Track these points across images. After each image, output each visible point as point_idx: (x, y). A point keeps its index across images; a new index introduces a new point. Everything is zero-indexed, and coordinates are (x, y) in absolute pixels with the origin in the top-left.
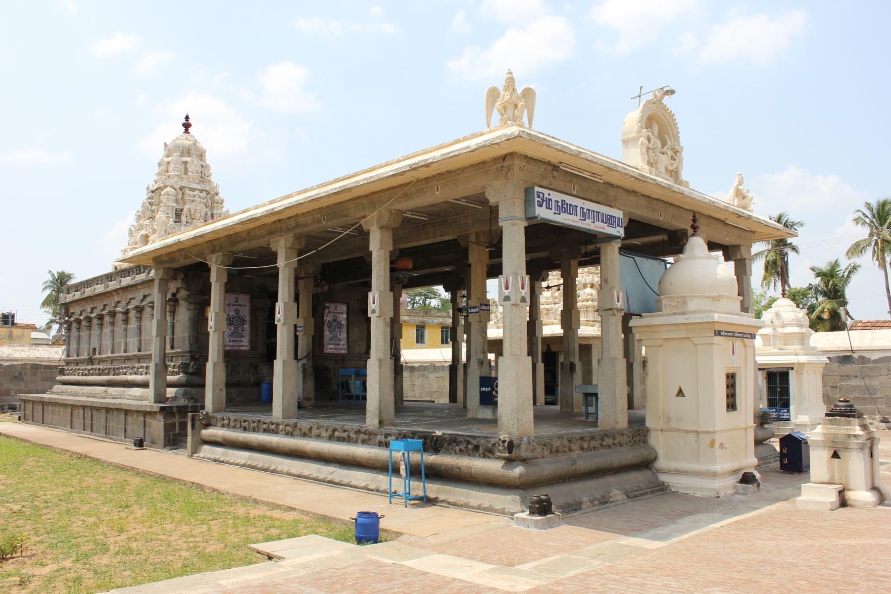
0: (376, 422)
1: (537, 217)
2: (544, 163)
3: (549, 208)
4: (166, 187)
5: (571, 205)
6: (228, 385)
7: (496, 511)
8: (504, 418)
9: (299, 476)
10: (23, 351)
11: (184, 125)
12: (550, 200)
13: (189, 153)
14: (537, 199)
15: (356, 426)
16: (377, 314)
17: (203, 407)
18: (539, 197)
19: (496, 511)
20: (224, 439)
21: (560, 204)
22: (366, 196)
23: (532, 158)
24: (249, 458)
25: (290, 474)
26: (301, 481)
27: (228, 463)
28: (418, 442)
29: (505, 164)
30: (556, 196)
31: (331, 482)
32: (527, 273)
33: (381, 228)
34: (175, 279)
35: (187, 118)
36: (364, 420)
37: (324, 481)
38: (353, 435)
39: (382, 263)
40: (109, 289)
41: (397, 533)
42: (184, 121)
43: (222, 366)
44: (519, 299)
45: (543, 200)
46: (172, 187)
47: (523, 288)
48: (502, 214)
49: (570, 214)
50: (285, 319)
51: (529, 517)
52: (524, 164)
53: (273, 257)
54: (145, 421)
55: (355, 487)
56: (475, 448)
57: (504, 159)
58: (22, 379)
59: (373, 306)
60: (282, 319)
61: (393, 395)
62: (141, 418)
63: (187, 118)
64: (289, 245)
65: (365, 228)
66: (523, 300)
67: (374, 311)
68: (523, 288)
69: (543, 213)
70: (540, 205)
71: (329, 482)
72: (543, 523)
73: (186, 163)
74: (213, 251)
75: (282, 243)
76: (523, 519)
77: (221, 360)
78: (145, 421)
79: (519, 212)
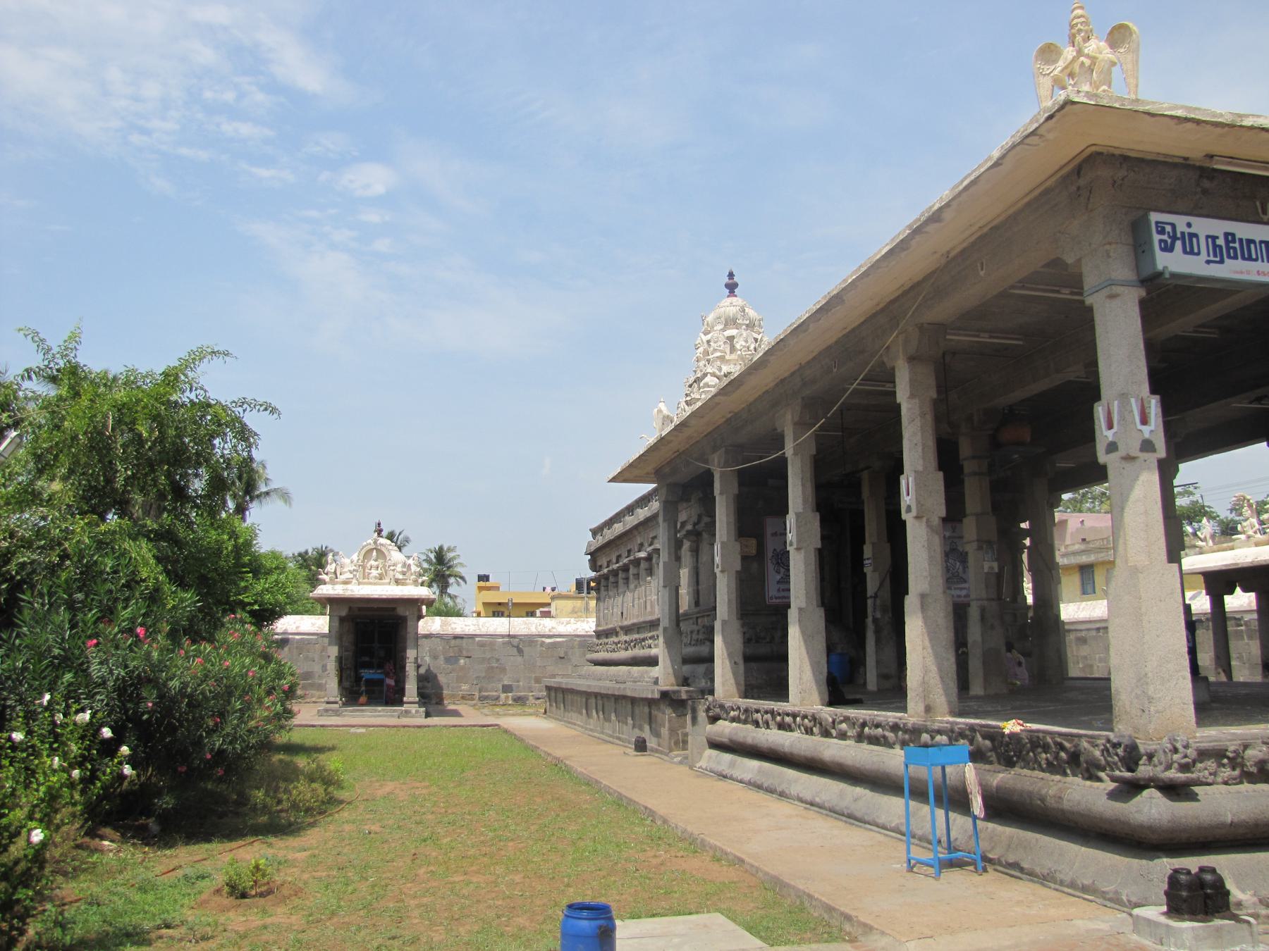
0: (921, 708)
1: (1160, 274)
2: (1175, 165)
3: (1192, 252)
4: (705, 375)
5: (1250, 242)
6: (747, 659)
7: (1103, 895)
8: (1123, 697)
9: (812, 804)
10: (568, 623)
11: (727, 286)
12: (1192, 235)
13: (735, 323)
14: (1156, 238)
15: (891, 716)
16: (914, 513)
17: (712, 692)
18: (1162, 232)
19: (1103, 895)
20: (731, 741)
21: (1221, 242)
22: (882, 310)
23: (1141, 160)
24: (760, 771)
25: (801, 800)
26: (812, 813)
27: (731, 778)
28: (964, 746)
29: (1082, 182)
30: (1205, 227)
31: (851, 818)
32: (1154, 391)
33: (912, 359)
34: (688, 500)
35: (731, 275)
36: (904, 709)
37: (843, 815)
38: (890, 735)
39: (918, 422)
40: (628, 527)
41: (865, 925)
42: (726, 280)
43: (736, 624)
44: (1137, 445)
45: (1174, 238)
46: (713, 375)
47: (1144, 421)
48: (1089, 281)
49: (1250, 258)
50: (799, 541)
51: (1163, 919)
52: (1122, 173)
53: (779, 441)
54: (650, 713)
55: (884, 827)
56: (1077, 762)
57: (1079, 173)
58: (569, 660)
59: (907, 499)
60: (794, 541)
61: (953, 660)
62: (646, 710)
63: (731, 275)
64: (796, 419)
65: (889, 365)
66: (1147, 446)
67: (909, 509)
68: (1144, 421)
69: (1173, 262)
70: (1168, 248)
71: (850, 816)
72: (1197, 938)
73: (731, 339)
74: (715, 449)
75: (789, 417)
76: (1149, 922)
77: (734, 617)
78: (650, 713)
79: (1122, 270)
